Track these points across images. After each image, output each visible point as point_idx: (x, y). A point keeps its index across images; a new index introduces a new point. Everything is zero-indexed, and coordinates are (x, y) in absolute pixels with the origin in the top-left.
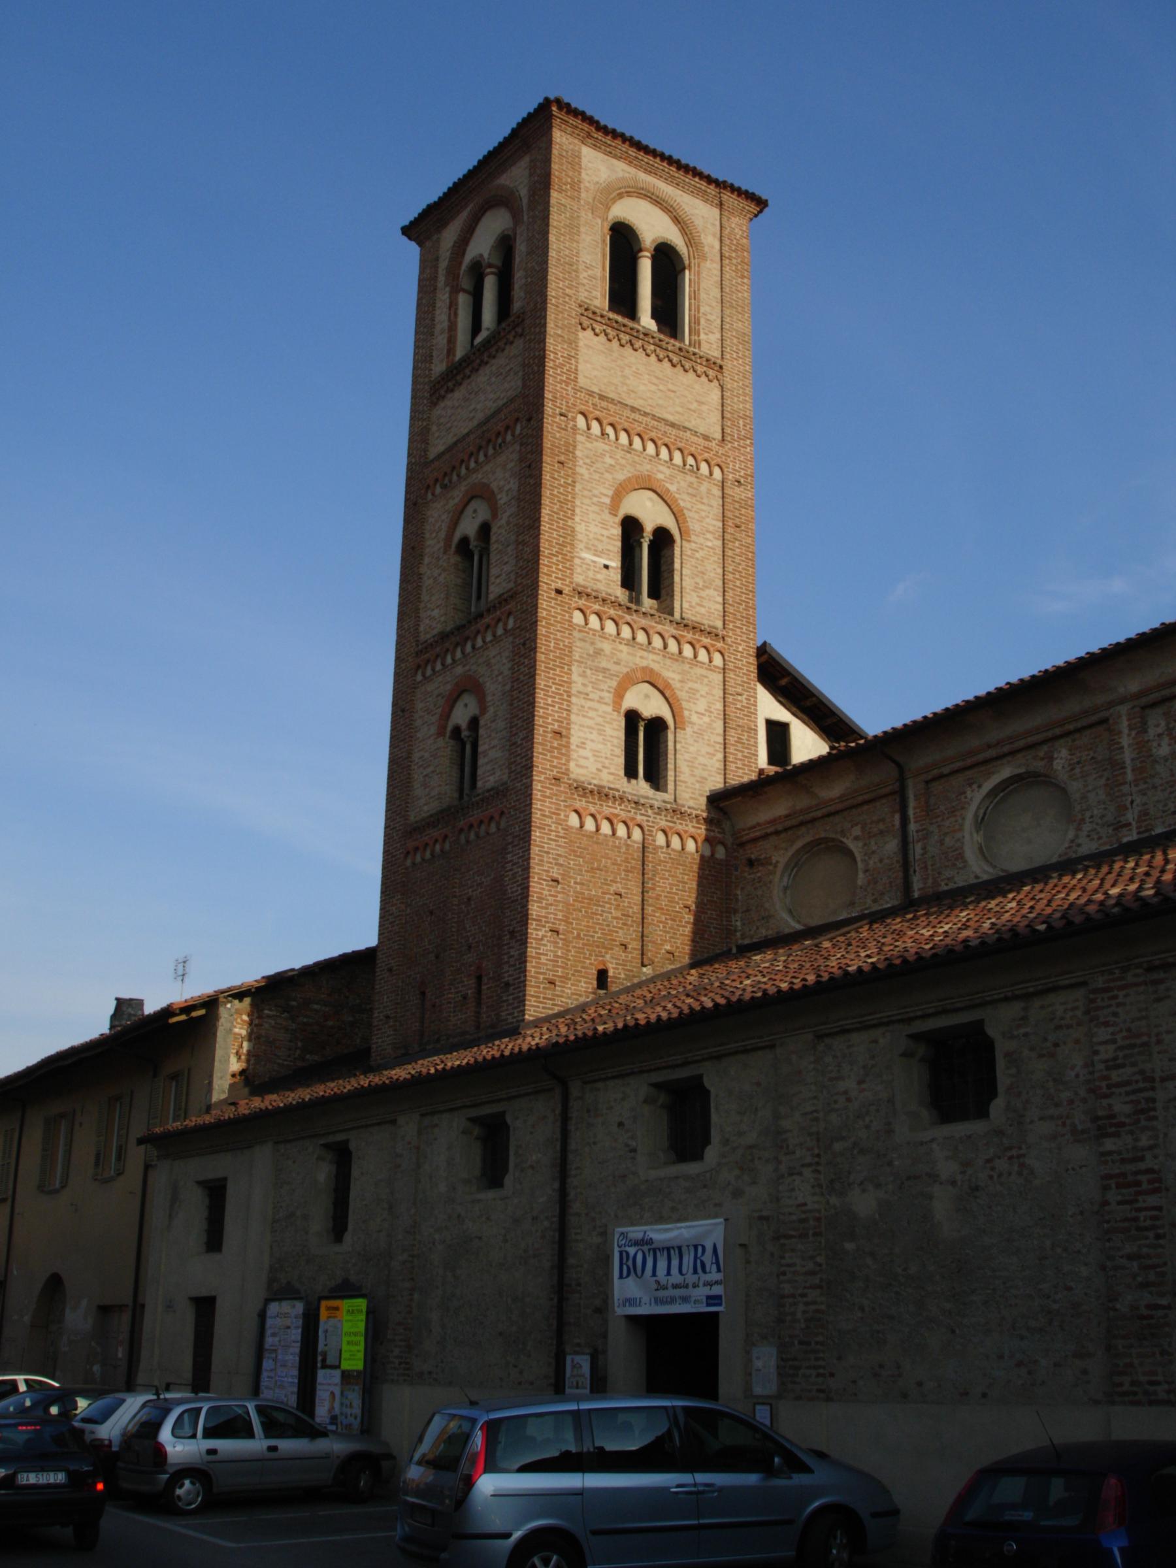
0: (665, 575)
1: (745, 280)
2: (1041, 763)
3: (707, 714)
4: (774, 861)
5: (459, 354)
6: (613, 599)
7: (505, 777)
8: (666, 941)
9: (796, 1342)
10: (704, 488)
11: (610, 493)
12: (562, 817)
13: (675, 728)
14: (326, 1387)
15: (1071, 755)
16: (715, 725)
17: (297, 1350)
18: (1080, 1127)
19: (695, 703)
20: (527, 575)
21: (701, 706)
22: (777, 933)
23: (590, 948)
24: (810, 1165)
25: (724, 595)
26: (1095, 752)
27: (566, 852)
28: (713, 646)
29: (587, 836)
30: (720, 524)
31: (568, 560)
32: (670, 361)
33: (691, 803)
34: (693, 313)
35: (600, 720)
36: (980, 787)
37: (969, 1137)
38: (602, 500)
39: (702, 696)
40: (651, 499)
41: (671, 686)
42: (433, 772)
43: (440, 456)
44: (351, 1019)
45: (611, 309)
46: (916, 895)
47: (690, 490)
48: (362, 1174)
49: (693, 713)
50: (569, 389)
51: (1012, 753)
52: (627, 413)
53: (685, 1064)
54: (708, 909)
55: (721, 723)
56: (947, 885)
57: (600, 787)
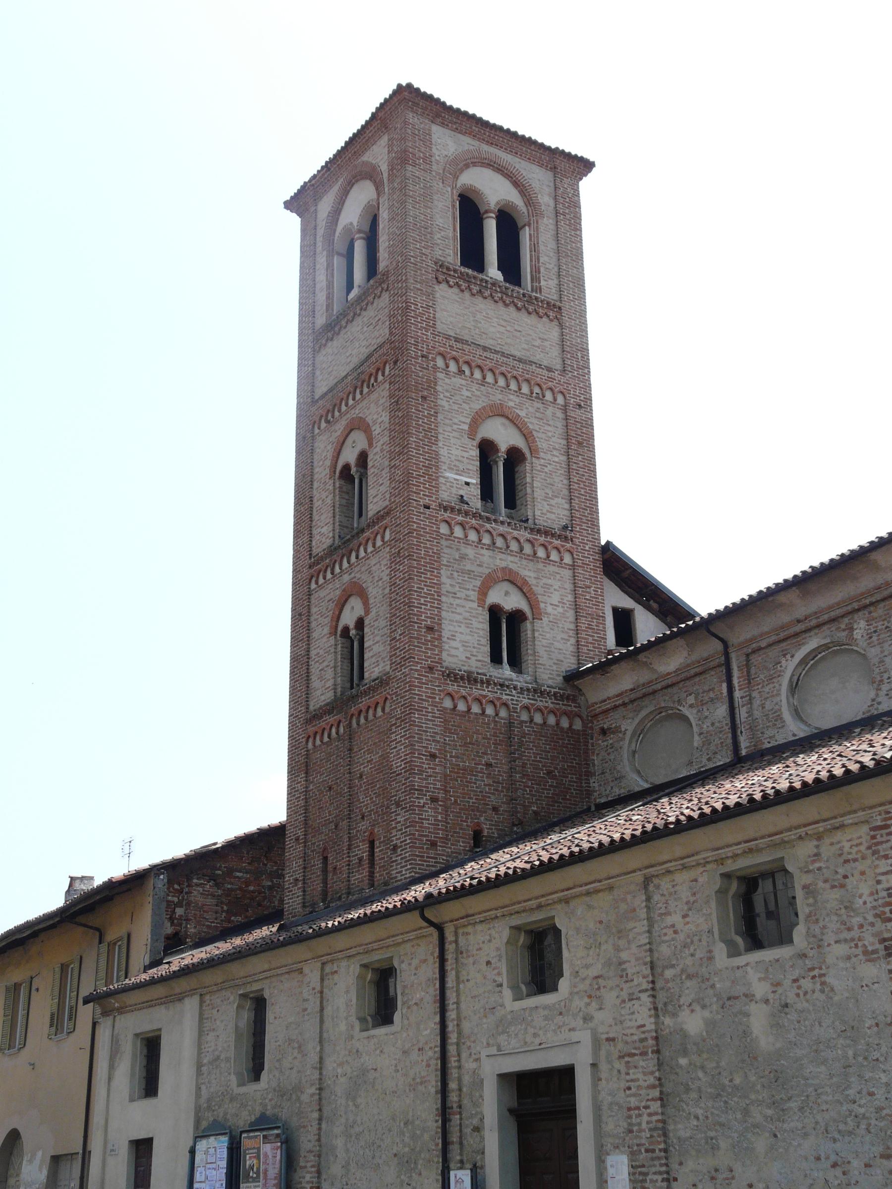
0: (520, 487)
2: (844, 634)
3: (561, 605)
4: (623, 730)
7: (388, 668)
8: (532, 803)
9: (643, 1151)
10: (549, 411)
11: (468, 421)
15: (868, 625)
16: (568, 614)
18: (870, 948)
19: (549, 596)
20: (399, 494)
21: (555, 598)
22: (629, 791)
23: (466, 812)
24: (646, 990)
26: (888, 622)
27: (441, 730)
28: (563, 546)
29: (460, 716)
31: (433, 480)
32: (516, 306)
33: (550, 682)
36: (792, 656)
37: (778, 960)
38: (460, 427)
39: (555, 590)
40: (504, 425)
41: (528, 583)
42: (327, 666)
43: (323, 397)
44: (270, 883)
45: (462, 264)
46: (744, 752)
47: (538, 415)
48: (275, 1018)
49: (548, 605)
50: (429, 334)
51: (818, 626)
52: (480, 352)
53: (540, 907)
54: (569, 774)
56: (769, 742)
57: (470, 673)
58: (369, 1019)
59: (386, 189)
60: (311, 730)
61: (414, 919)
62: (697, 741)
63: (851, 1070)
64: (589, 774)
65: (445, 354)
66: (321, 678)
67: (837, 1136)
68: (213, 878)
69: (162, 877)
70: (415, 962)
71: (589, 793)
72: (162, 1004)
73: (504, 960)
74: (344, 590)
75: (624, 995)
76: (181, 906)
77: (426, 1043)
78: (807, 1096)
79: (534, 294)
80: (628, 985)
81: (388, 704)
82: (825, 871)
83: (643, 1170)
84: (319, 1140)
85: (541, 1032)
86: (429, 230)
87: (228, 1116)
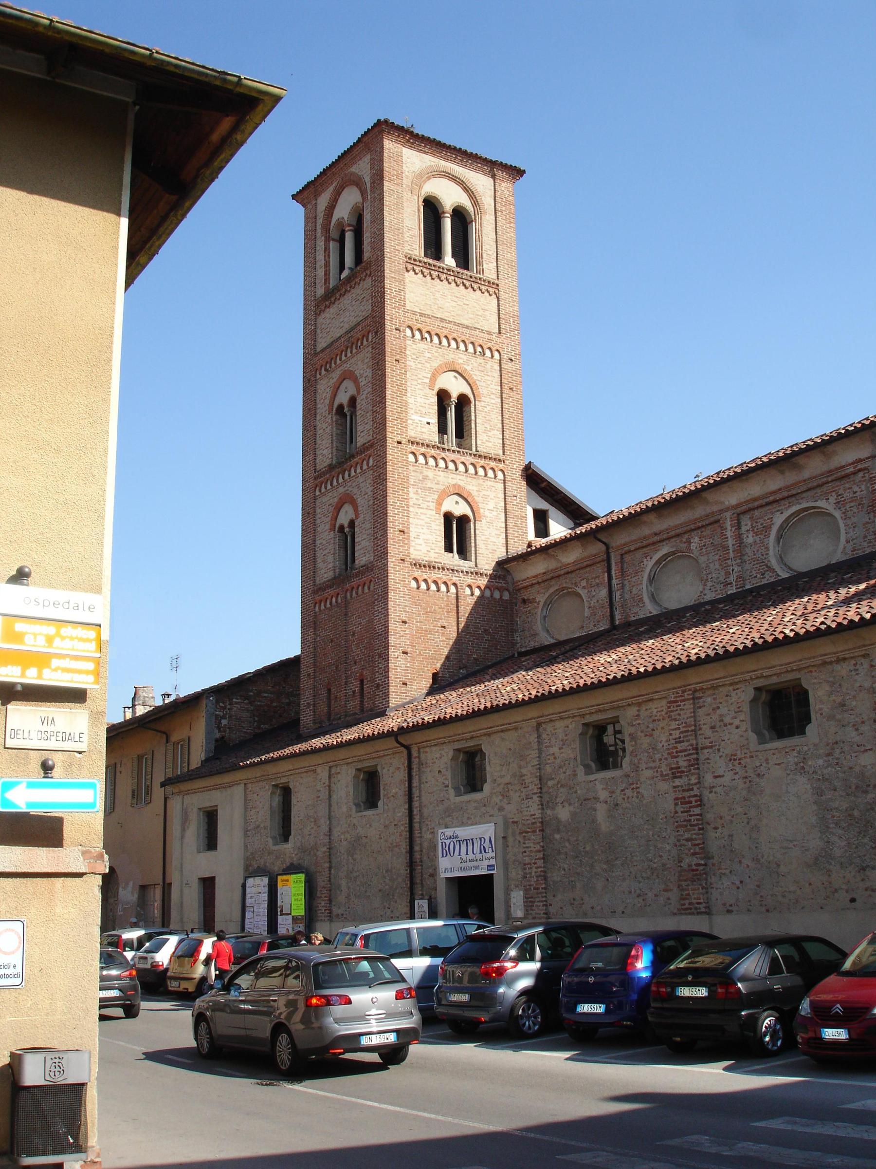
0: (466, 423)
1: (512, 225)
2: (685, 545)
5: (332, 284)
6: (433, 444)
7: (372, 558)
11: (429, 376)
12: (407, 582)
13: (475, 521)
14: (284, 926)
17: (266, 906)
18: (664, 773)
21: (491, 505)
24: (537, 793)
25: (503, 434)
28: (497, 467)
30: (499, 388)
34: (478, 251)
35: (428, 520)
36: (651, 558)
37: (613, 778)
40: (455, 377)
42: (329, 553)
43: (323, 350)
44: (287, 701)
45: (426, 255)
46: (617, 623)
47: (480, 368)
51: (669, 538)
52: (438, 323)
53: (472, 738)
55: (503, 514)
58: (362, 804)
59: (369, 197)
60: (318, 598)
61: (391, 743)
62: (587, 613)
63: (651, 843)
64: (515, 631)
65: (412, 326)
66: (324, 561)
67: (641, 879)
68: (246, 698)
69: (211, 698)
70: (392, 769)
71: (514, 644)
72: (217, 789)
73: (449, 770)
74: (340, 498)
75: (523, 795)
76: (225, 719)
77: (400, 821)
78: (626, 858)
79: (478, 275)
80: (525, 790)
81: (372, 584)
82: (642, 725)
83: (532, 899)
84: (329, 881)
85: (472, 817)
86: (401, 231)
87: (267, 864)
